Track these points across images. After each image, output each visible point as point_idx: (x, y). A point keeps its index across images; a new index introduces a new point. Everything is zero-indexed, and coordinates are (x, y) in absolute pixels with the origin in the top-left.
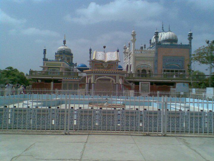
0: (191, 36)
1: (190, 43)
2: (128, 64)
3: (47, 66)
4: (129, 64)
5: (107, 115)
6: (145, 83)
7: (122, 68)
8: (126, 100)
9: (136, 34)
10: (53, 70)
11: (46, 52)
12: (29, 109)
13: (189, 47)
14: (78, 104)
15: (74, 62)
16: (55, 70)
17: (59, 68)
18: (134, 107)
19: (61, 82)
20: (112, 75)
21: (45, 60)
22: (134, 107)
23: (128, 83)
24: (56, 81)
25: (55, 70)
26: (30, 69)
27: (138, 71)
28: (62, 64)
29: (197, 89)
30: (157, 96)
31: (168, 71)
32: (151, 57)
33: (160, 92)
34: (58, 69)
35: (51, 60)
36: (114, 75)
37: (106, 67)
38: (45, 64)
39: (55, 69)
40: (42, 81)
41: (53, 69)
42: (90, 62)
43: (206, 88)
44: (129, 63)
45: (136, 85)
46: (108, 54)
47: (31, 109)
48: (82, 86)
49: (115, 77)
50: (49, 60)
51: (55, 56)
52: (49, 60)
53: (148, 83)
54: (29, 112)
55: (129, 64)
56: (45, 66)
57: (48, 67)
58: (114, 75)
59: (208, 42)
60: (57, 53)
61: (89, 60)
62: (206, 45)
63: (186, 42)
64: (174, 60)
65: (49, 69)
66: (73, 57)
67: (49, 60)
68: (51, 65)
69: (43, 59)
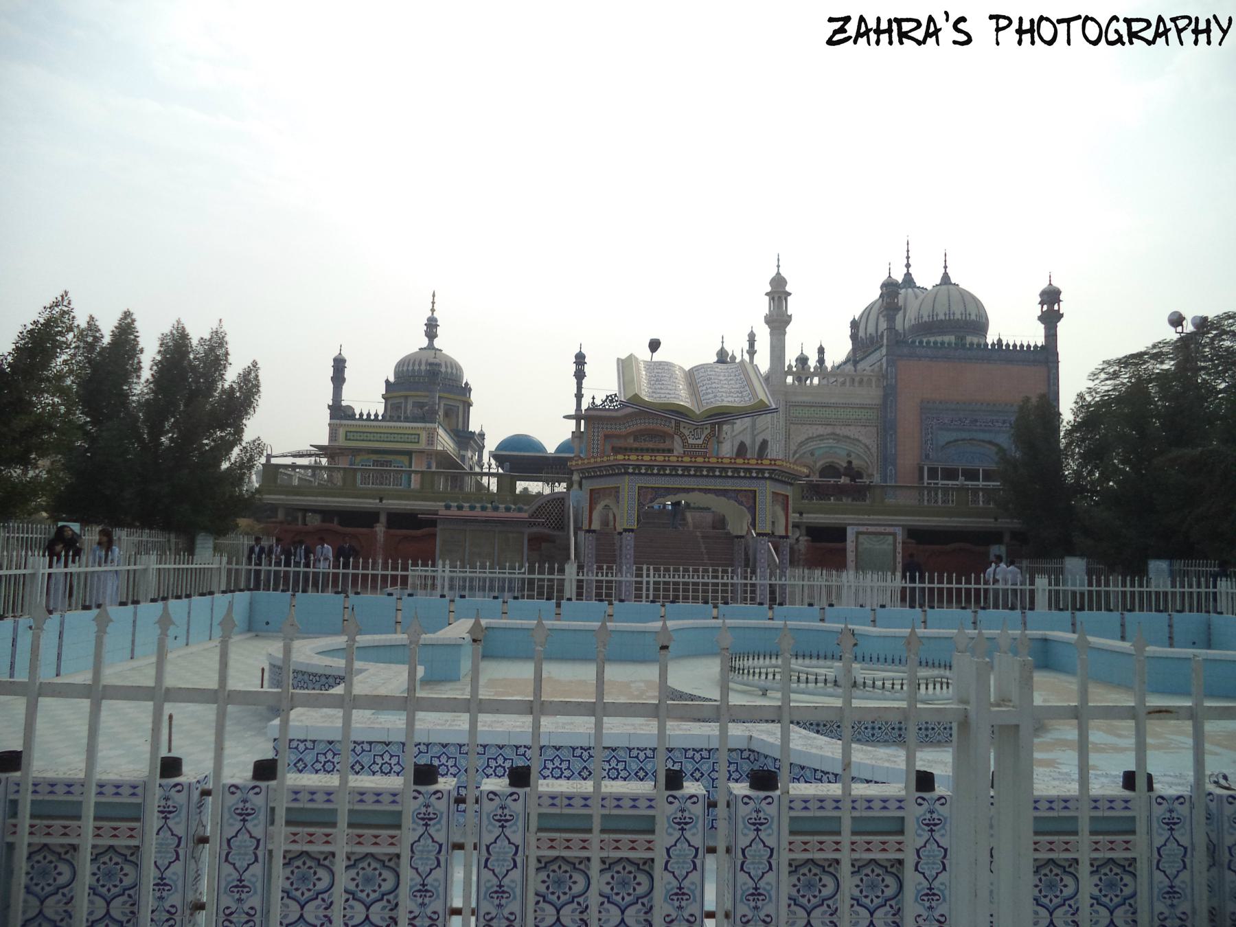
1: (1051, 335)
4: (754, 442)
5: (1085, 855)
6: (873, 531)
8: (921, 631)
10: (376, 463)
11: (348, 374)
12: (180, 799)
13: (1044, 358)
14: (584, 659)
15: (474, 427)
16: (389, 463)
17: (409, 453)
19: (433, 523)
20: (729, 485)
21: (339, 411)
24: (400, 520)
25: (389, 463)
26: (178, 322)
29: (1179, 565)
31: (950, 474)
32: (862, 407)
33: (229, 562)
34: (405, 459)
35: (369, 415)
36: (745, 485)
37: (700, 442)
38: (342, 432)
40: (323, 521)
41: (374, 457)
42: (578, 425)
43: (1062, 557)
44: (754, 437)
45: (818, 545)
47: (206, 793)
48: (544, 545)
49: (750, 501)
50: (361, 415)
52: (361, 415)
53: (894, 535)
54: (180, 830)
55: (754, 442)
56: (342, 442)
58: (745, 485)
59: (1176, 320)
60: (392, 379)
61: (572, 411)
62: (1172, 335)
63: (1035, 335)
64: (976, 421)
66: (470, 405)
67: (357, 412)
69: (329, 407)
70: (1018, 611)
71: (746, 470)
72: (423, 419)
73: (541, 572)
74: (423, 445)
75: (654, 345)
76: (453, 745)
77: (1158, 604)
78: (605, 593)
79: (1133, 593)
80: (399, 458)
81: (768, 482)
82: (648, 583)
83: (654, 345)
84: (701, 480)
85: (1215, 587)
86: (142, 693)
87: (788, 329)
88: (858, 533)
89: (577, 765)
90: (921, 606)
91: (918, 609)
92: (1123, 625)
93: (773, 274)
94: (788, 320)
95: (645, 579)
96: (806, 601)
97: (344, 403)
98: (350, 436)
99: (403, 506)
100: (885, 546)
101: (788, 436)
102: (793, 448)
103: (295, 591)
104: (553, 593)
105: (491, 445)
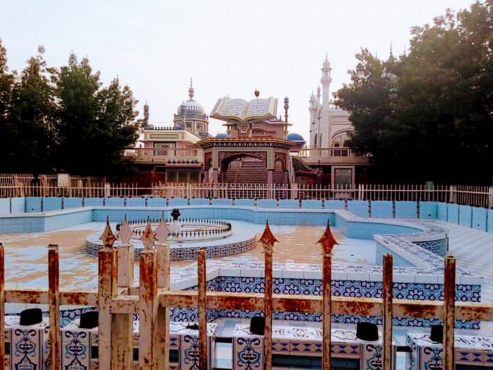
0: (324, 237)
2: (317, 132)
3: (152, 140)
7: (303, 140)
9: (331, 67)
10: (163, 146)
17: (175, 142)
18: (268, 264)
22: (268, 264)
23: (309, 170)
27: (337, 145)
28: (180, 134)
30: (357, 198)
33: (365, 188)
38: (149, 135)
39: (167, 144)
46: (76, 90)
51: (175, 122)
53: (351, 169)
56: (149, 139)
57: (155, 142)
60: (177, 114)
65: (156, 145)
68: (159, 136)
70: (391, 202)
71: (267, 143)
72: (180, 129)
73: (389, 189)
74: (180, 139)
75: (257, 94)
76: (421, 284)
77: (100, 194)
78: (279, 196)
79: (96, 190)
80: (171, 145)
81: (272, 148)
82: (361, 192)
83: (257, 94)
84: (229, 148)
85: (104, 187)
86: (41, 236)
87: (330, 85)
88: (335, 169)
89: (428, 293)
90: (368, 199)
91: (367, 201)
92: (394, 207)
93: (324, 61)
94: (330, 81)
95: (360, 190)
96: (184, 196)
97: (149, 124)
98: (152, 136)
99: (246, 157)
100: (347, 174)
101: (330, 129)
102: (332, 135)
103: (418, 200)
104: (101, 195)
105: (289, 133)
